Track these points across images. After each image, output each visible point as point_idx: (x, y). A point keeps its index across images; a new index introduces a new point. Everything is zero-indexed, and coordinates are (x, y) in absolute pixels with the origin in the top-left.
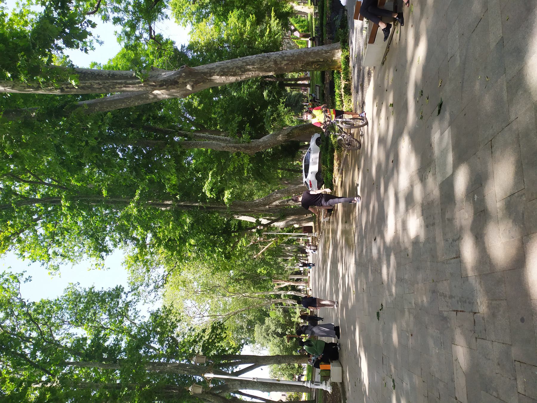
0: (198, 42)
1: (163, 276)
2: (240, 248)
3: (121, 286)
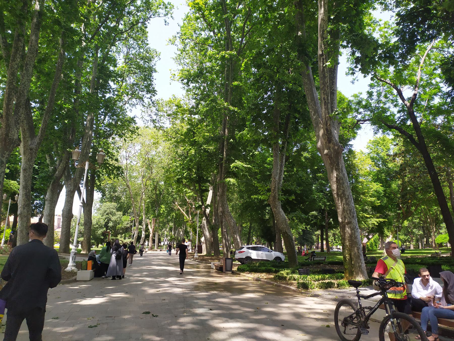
0: (355, 158)
1: (163, 127)
2: (185, 190)
3: (157, 94)
